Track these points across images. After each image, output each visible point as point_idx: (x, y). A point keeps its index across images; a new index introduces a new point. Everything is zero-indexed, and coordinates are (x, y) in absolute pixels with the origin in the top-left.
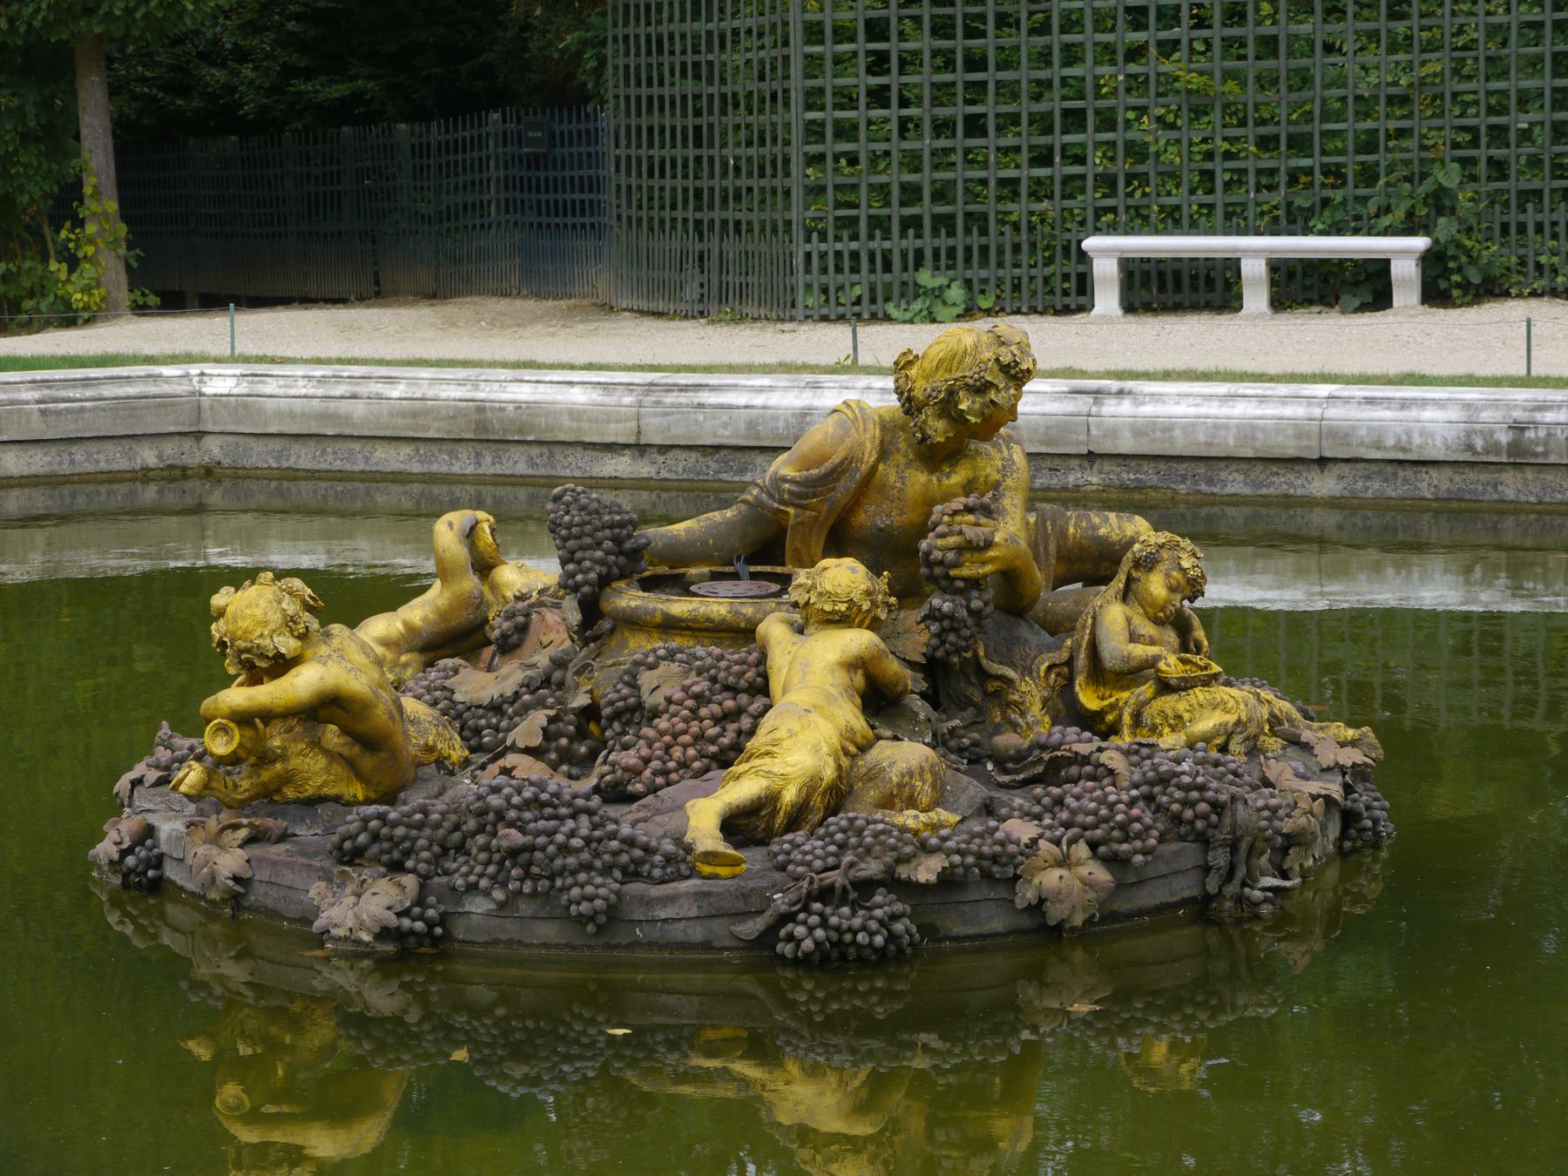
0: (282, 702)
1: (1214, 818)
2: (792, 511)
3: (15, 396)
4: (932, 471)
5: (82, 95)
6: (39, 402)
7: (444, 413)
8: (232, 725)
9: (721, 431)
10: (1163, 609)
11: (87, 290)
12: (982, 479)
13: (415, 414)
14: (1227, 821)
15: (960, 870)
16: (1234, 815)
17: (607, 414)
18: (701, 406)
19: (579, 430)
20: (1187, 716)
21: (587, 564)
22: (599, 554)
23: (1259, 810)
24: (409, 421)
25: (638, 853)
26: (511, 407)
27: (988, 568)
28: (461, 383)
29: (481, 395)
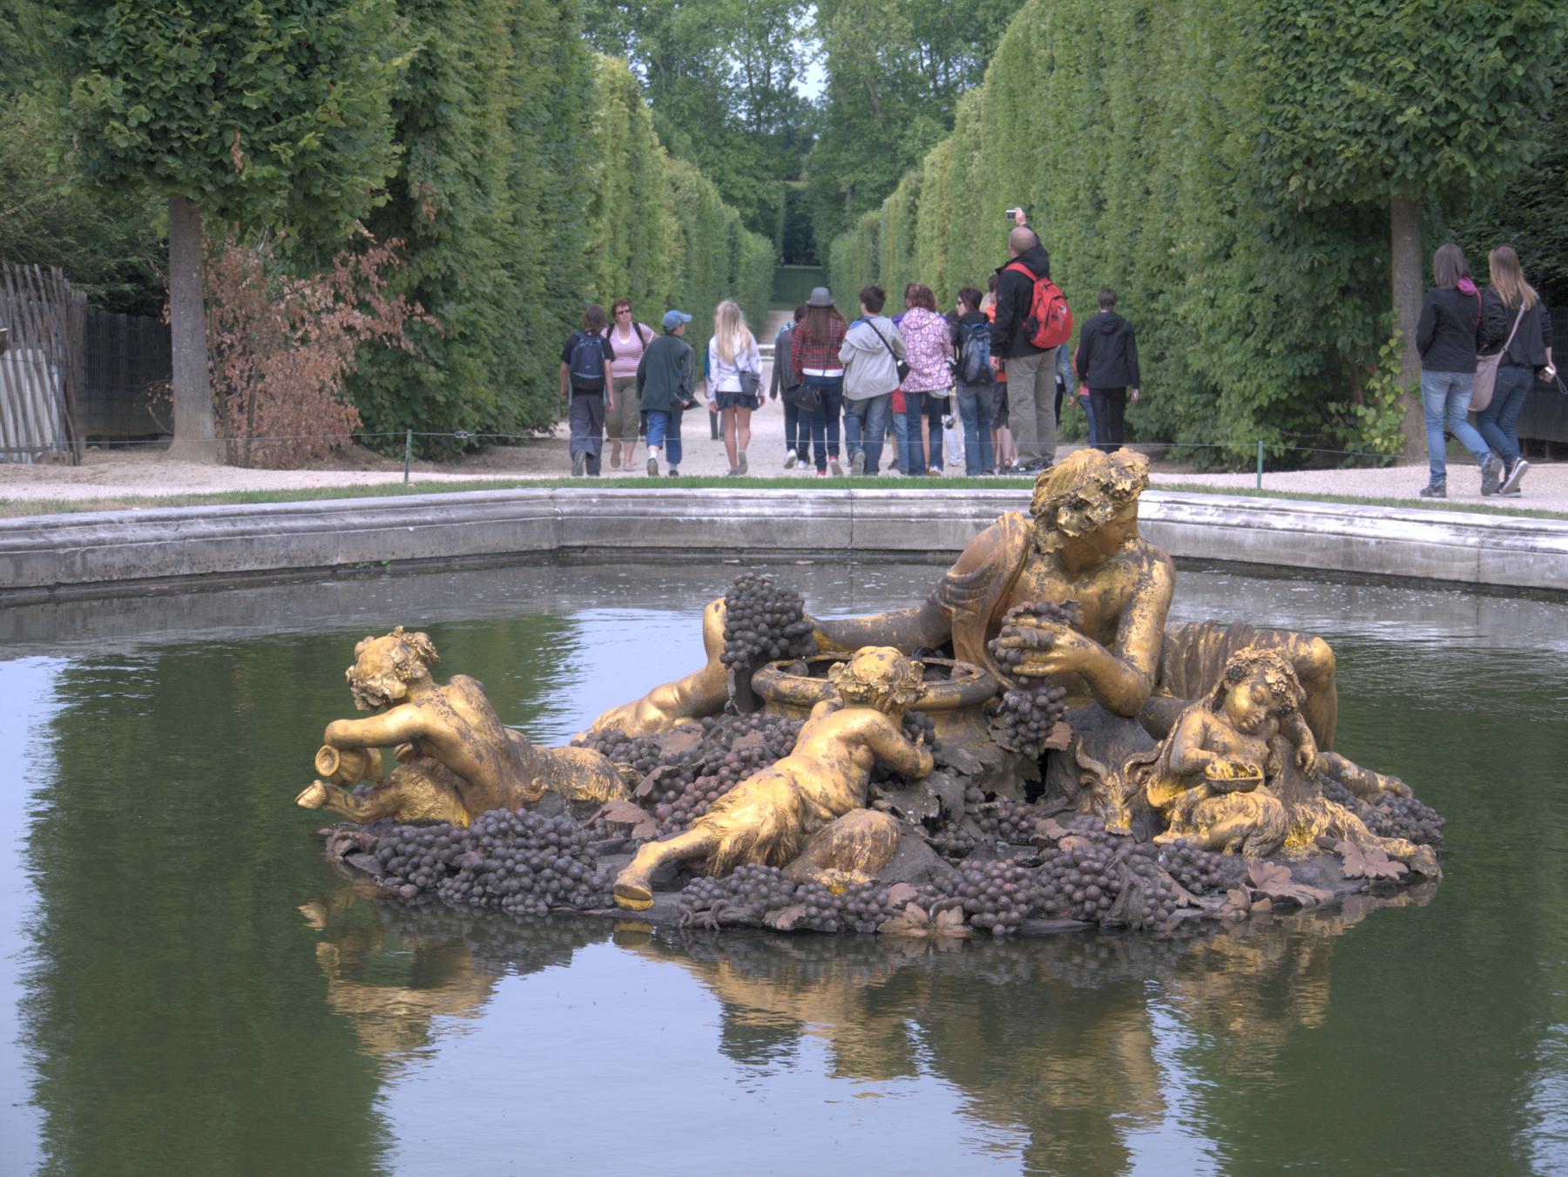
0: (371, 735)
1: (1104, 901)
2: (953, 609)
3: (955, 510)
4: (1070, 581)
5: (1396, 253)
6: (975, 516)
7: (1318, 544)
8: (335, 751)
9: (1549, 575)
10: (1245, 719)
11: (1385, 435)
12: (1118, 591)
13: (1294, 544)
14: (1119, 905)
15: (817, 921)
16: (1127, 901)
17: (1453, 553)
18: (1533, 549)
19: (1428, 567)
20: (1219, 817)
21: (740, 643)
22: (751, 635)
23: (1147, 897)
24: (1289, 551)
25: (568, 881)
26: (1373, 542)
27: (1051, 668)
28: (1339, 518)
29: (1349, 530)
